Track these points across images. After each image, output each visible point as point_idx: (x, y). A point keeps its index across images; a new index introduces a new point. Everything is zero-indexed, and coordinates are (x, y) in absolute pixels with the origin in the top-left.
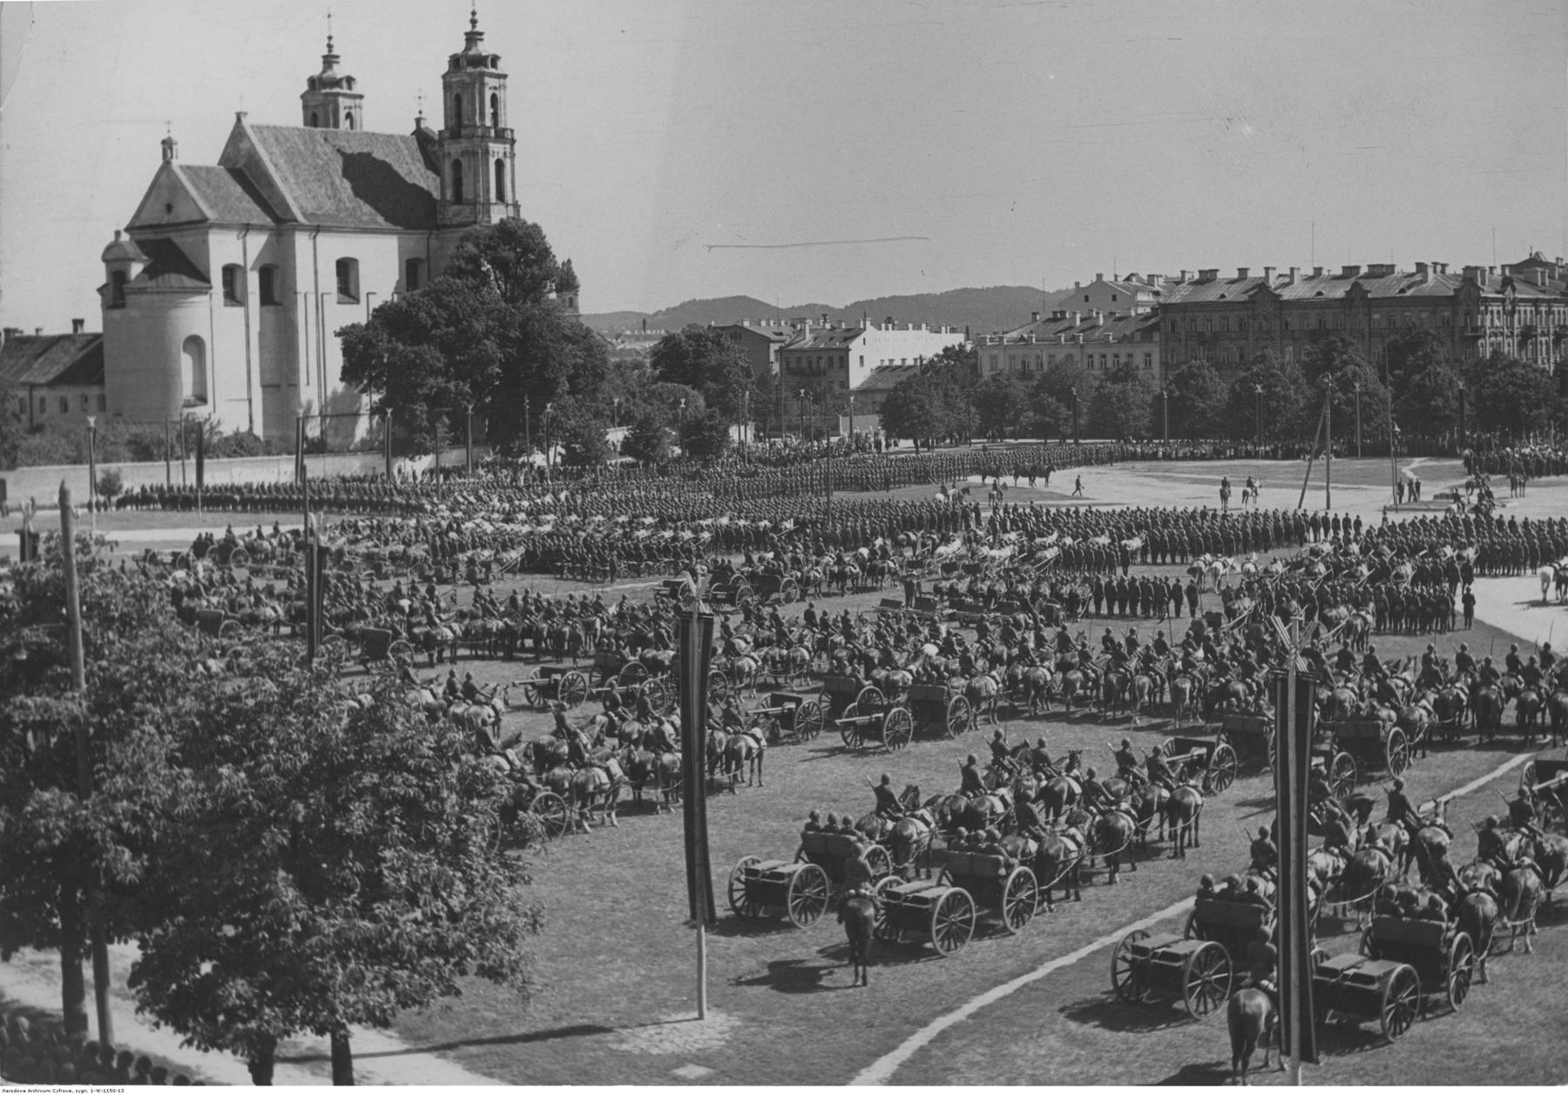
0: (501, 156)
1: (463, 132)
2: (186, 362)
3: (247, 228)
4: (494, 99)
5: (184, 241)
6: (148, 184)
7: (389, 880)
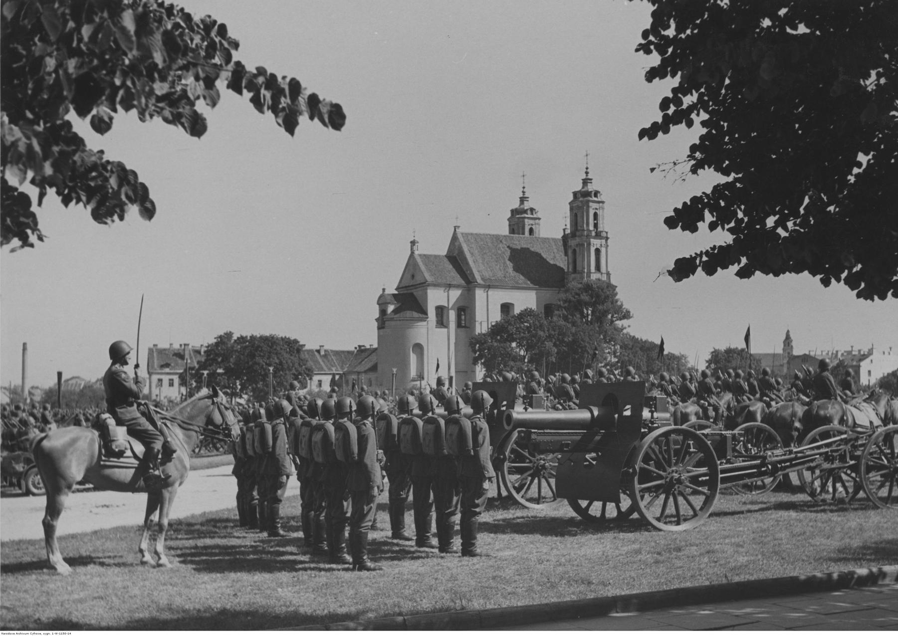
0: (598, 247)
1: (578, 233)
2: (413, 358)
3: (449, 286)
4: (596, 215)
5: (417, 293)
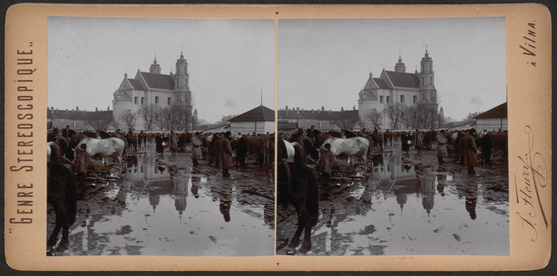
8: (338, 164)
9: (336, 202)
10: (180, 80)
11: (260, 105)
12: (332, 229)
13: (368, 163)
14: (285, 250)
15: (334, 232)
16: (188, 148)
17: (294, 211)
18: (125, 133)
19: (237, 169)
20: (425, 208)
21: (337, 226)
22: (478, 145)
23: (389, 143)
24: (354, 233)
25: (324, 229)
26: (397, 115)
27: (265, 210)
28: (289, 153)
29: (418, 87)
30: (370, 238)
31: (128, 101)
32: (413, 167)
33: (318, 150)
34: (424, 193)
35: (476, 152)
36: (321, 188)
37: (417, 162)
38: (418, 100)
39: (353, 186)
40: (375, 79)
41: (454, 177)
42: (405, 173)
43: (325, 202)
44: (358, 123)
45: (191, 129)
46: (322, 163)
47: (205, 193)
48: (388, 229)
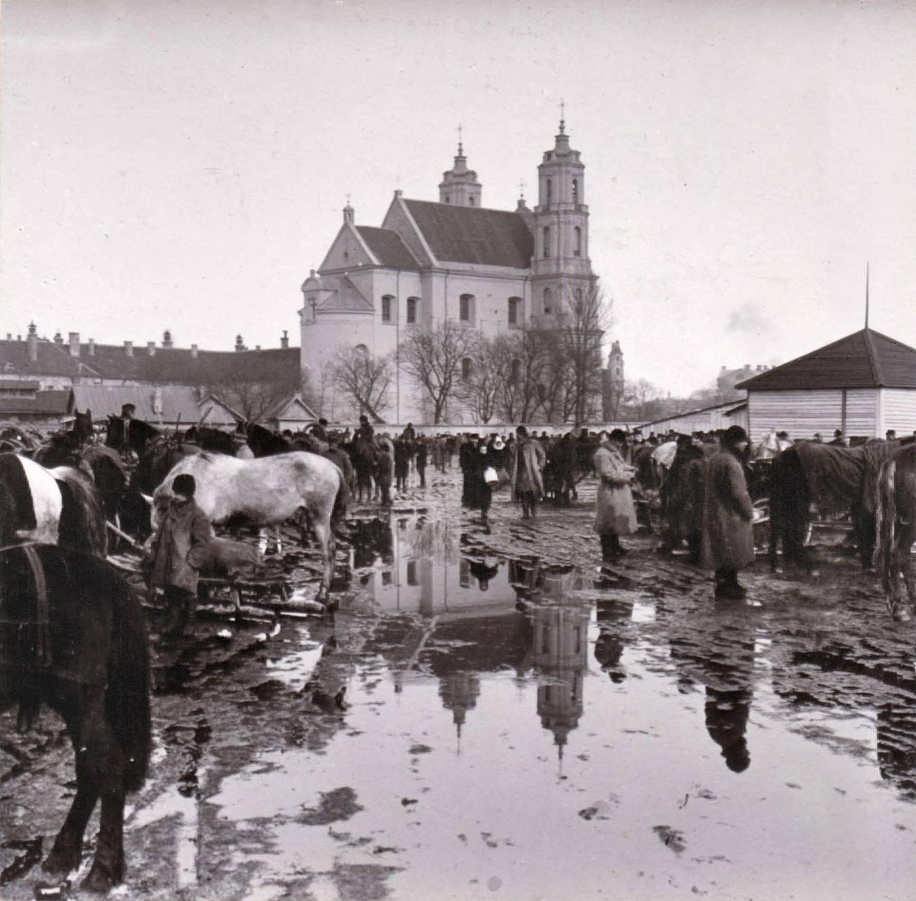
1: (554, 208)
6: (329, 247)
7: (766, 551)
8: (225, 556)
9: (215, 698)
10: (555, 228)
11: (861, 327)
12: (201, 803)
13: (333, 552)
14: (30, 883)
15: (208, 814)
16: (586, 491)
17: (62, 733)
18: (347, 433)
19: (773, 570)
20: (546, 725)
21: (218, 792)
22: (756, 491)
23: (413, 479)
24: (281, 820)
25: (172, 802)
26: (448, 370)
27: (881, 729)
28: (39, 510)
29: (527, 265)
30: (337, 837)
31: (354, 311)
32: (504, 571)
33: (149, 499)
34: (546, 670)
35: (746, 517)
36: (158, 649)
37: (519, 551)
38: (527, 311)
39: (279, 639)
40: (365, 231)
41: (660, 609)
42: (474, 593)
43: (176, 700)
44: (298, 396)
45: (599, 417)
46: (163, 552)
47: (644, 662)
48: (405, 802)
